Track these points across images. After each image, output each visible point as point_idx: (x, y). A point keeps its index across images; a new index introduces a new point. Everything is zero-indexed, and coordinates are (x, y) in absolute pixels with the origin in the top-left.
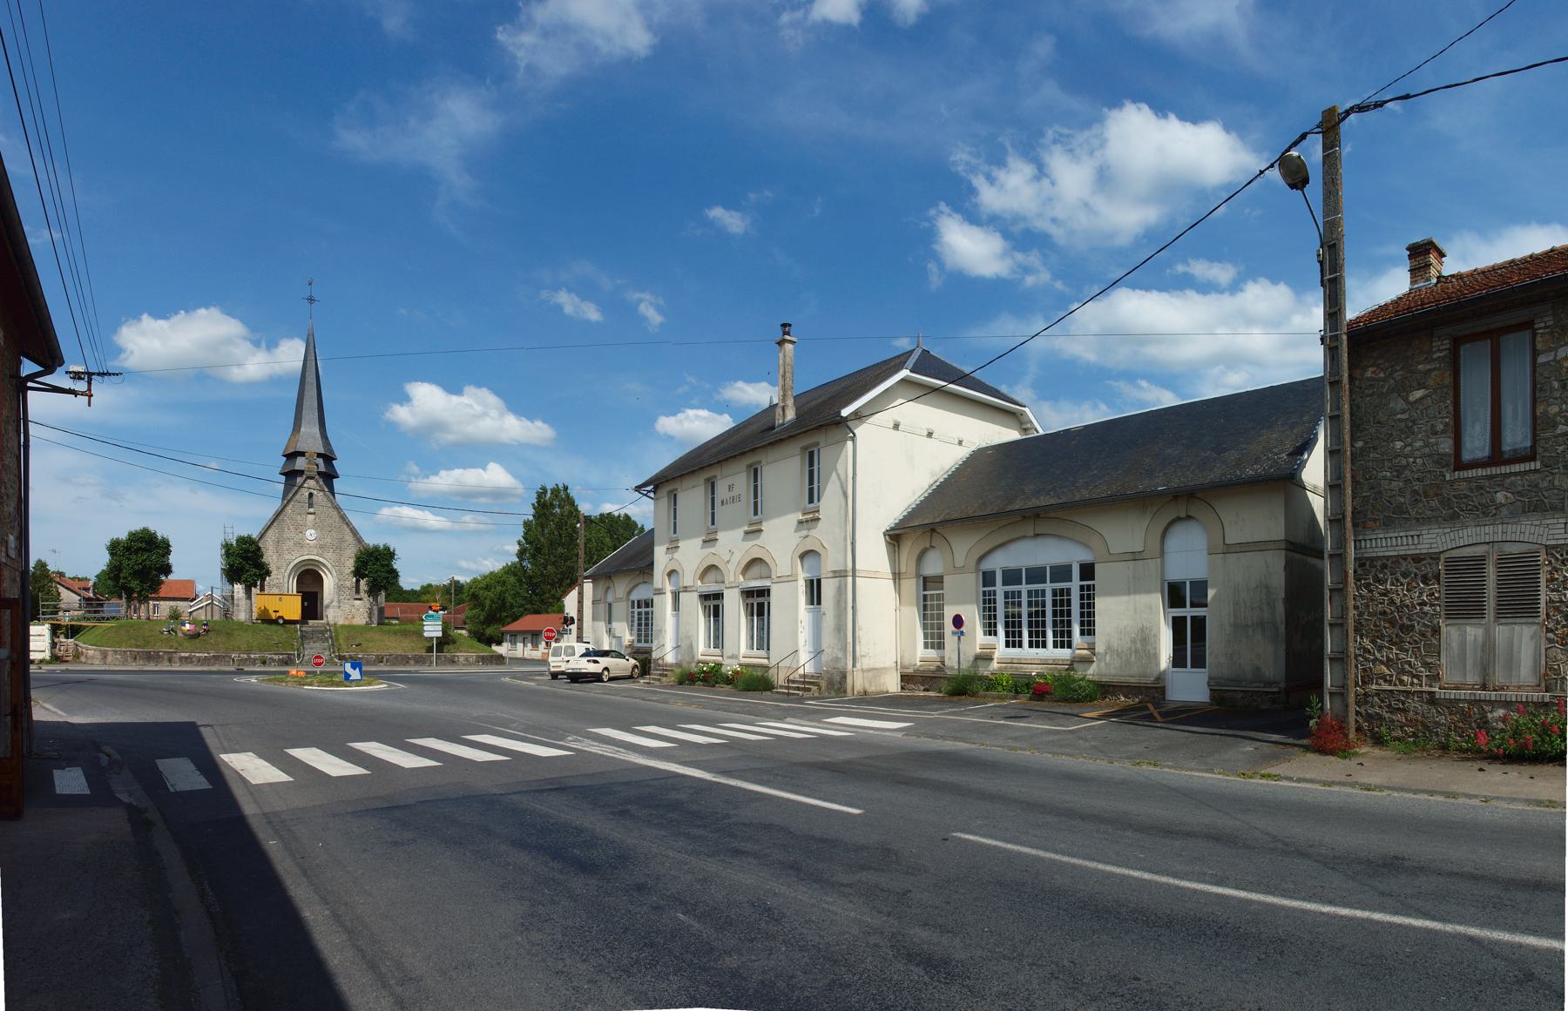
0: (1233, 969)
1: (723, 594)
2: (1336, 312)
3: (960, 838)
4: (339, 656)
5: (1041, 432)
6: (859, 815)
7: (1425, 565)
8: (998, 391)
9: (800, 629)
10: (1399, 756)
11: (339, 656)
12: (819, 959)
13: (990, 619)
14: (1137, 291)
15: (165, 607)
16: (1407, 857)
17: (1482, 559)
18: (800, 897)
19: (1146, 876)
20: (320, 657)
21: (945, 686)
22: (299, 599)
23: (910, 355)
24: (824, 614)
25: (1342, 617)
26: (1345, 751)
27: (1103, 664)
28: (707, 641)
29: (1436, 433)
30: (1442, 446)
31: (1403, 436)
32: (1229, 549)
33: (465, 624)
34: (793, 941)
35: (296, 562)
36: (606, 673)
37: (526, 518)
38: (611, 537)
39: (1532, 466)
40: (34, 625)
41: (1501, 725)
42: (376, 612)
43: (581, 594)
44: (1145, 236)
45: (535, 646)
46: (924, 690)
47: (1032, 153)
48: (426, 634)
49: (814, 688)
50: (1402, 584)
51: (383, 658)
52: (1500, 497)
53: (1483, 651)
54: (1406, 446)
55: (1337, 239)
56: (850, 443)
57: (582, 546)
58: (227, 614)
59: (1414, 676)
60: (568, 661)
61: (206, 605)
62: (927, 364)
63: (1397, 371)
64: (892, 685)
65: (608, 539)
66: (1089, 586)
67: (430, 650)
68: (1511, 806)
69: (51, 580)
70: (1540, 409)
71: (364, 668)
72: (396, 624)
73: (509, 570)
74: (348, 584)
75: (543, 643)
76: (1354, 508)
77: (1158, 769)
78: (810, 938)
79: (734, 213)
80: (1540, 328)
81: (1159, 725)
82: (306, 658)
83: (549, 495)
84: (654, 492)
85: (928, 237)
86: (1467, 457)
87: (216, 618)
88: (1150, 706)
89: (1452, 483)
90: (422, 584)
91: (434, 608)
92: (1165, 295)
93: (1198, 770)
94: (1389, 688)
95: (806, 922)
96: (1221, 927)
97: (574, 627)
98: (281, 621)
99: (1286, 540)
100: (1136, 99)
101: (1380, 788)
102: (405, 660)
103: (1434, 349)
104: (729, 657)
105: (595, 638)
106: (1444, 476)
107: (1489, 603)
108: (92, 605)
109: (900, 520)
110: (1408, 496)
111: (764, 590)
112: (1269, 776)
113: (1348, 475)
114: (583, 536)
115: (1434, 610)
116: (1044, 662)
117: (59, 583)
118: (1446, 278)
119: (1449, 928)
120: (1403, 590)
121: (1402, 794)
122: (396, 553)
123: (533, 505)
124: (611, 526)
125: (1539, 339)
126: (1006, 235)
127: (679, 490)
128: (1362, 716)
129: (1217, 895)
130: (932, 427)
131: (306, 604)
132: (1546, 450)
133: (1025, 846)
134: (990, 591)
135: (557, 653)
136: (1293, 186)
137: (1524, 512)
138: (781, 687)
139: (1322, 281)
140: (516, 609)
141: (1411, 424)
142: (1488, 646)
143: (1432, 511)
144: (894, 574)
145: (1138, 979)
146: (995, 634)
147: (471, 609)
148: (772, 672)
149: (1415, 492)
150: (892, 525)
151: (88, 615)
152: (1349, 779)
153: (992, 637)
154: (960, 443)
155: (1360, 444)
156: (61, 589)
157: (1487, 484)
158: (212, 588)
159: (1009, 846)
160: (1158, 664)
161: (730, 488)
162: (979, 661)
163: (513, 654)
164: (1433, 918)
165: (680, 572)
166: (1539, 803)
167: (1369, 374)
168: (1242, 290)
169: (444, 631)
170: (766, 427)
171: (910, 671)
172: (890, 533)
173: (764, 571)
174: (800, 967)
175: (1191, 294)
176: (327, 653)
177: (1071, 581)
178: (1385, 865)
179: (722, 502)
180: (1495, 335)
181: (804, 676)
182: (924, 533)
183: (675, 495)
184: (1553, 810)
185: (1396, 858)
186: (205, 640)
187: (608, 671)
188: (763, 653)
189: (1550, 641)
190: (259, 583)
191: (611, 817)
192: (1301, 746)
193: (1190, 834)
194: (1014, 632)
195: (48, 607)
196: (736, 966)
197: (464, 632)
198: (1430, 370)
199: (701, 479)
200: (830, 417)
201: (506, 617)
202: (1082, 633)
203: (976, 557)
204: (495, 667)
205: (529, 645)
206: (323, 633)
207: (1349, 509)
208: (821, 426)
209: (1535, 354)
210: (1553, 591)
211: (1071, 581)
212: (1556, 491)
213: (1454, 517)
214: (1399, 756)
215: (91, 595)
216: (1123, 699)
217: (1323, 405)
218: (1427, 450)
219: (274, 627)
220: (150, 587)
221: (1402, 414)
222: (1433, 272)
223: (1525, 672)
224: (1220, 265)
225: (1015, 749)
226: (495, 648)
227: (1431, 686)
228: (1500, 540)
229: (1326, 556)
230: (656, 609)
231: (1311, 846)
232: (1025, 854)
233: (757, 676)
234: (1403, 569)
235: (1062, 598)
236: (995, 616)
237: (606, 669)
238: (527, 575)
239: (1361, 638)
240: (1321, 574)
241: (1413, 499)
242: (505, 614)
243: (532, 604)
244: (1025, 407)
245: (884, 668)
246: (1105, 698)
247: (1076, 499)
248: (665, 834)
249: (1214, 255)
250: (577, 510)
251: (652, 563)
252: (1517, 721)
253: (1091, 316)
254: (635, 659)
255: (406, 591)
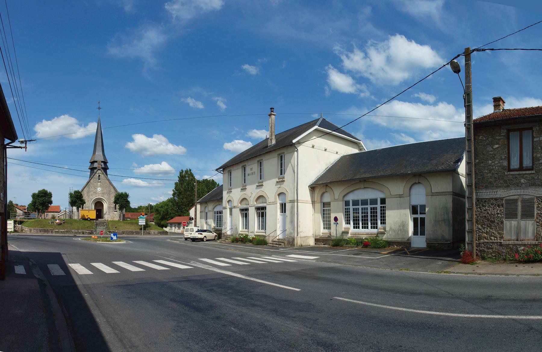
0: (435, 340)
1: (248, 209)
2: (470, 116)
3: (337, 299)
4: (109, 231)
5: (366, 150)
6: (299, 291)
7: (498, 201)
8: (351, 135)
9: (278, 222)
10: (490, 263)
11: (109, 231)
12: (284, 345)
13: (348, 218)
14: (401, 102)
15: (50, 215)
16: (493, 296)
17: (517, 200)
18: (277, 322)
19: (404, 309)
20: (102, 232)
21: (331, 243)
22: (95, 212)
23: (318, 120)
24: (287, 216)
25: (472, 218)
26: (472, 262)
27: (389, 234)
28: (243, 226)
29: (502, 159)
30: (504, 163)
31: (492, 159)
32: (433, 194)
33: (154, 220)
34: (274, 338)
35: (94, 199)
36: (205, 238)
37: (176, 181)
38: (207, 188)
39: (532, 172)
40: (9, 220)
41: (523, 252)
42: (122, 216)
43: (196, 209)
44: (404, 83)
45: (179, 228)
46: (324, 244)
47: (363, 48)
48: (140, 224)
49: (283, 244)
50: (491, 207)
51: (124, 232)
52: (522, 181)
53: (517, 229)
54: (492, 162)
55: (470, 92)
56: (296, 153)
57: (196, 192)
58: (71, 217)
59: (495, 237)
60: (191, 234)
61: (64, 214)
62: (325, 124)
63: (490, 138)
64: (312, 243)
65: (206, 189)
66: (383, 206)
67: (141, 229)
68: (526, 277)
69: (14, 207)
70: (535, 155)
71: (118, 236)
72: (129, 220)
73: (170, 201)
74: (112, 206)
75: (182, 227)
76: (475, 182)
77: (408, 271)
78: (281, 337)
79: (252, 67)
80: (535, 130)
81: (409, 256)
82: (98, 232)
83: (184, 173)
84: (223, 171)
85: (325, 77)
86: (512, 168)
87: (67, 218)
88: (406, 249)
89: (507, 175)
90: (138, 206)
91: (142, 214)
92: (411, 104)
93: (422, 271)
94: (487, 241)
95: (280, 331)
96: (430, 325)
97: (193, 221)
98: (89, 219)
99: (452, 192)
100: (401, 33)
101: (484, 274)
102: (132, 233)
103: (501, 132)
104: (251, 232)
105: (201, 225)
106: (505, 173)
107: (519, 213)
108: (27, 214)
109: (315, 181)
110: (493, 178)
111: (264, 207)
112: (447, 272)
113: (474, 171)
114: (197, 187)
115: (502, 216)
116: (367, 234)
117: (16, 208)
118: (505, 110)
119: (506, 317)
120: (491, 209)
121: (491, 275)
122: (129, 195)
123: (178, 176)
124: (207, 184)
125: (534, 133)
126: (354, 78)
127: (232, 170)
128: (478, 250)
129: (429, 314)
130: (326, 147)
131: (97, 213)
132: (536, 167)
133: (360, 301)
134: (347, 208)
135: (187, 231)
136: (455, 72)
137: (530, 186)
138: (270, 243)
139: (465, 105)
140: (172, 215)
141: (494, 156)
142: (519, 227)
143: (501, 184)
144: (312, 201)
145: (402, 346)
146: (350, 224)
147: (156, 215)
148: (267, 238)
149: (495, 178)
150: (312, 183)
151: (25, 218)
152: (474, 272)
153: (349, 225)
154: (337, 153)
155: (477, 161)
156: (17, 209)
157: (518, 176)
158: (66, 208)
159: (355, 301)
160: (408, 234)
161: (251, 169)
162: (343, 234)
163: (171, 231)
164: (501, 315)
165: (233, 202)
166: (534, 275)
167: (480, 138)
168: (437, 105)
169: (146, 223)
170: (264, 146)
171: (318, 237)
172: (311, 186)
173: (264, 201)
174: (277, 348)
175: (420, 104)
176: (105, 230)
177: (377, 205)
178: (486, 299)
179: (248, 175)
180: (521, 130)
181: (279, 239)
182: (323, 186)
183: (231, 172)
184: (539, 277)
185: (489, 296)
186: (63, 226)
187: (206, 237)
188: (263, 231)
189: (538, 225)
190: (81, 206)
191: (207, 291)
192: (458, 261)
193: (419, 294)
194: (356, 223)
195: (13, 215)
196: (253, 347)
197: (153, 223)
198: (500, 139)
199: (240, 167)
200: (289, 143)
201: (169, 217)
202: (381, 223)
203: (343, 195)
204: (164, 236)
205: (177, 228)
206: (103, 223)
207: (474, 182)
208: (285, 146)
209: (533, 138)
210: (538, 210)
211: (377, 205)
212: (539, 180)
213: (508, 186)
214: (490, 263)
215: (26, 211)
216: (396, 247)
217: (465, 147)
218: (499, 164)
219: (87, 221)
220: (45, 208)
221: (491, 152)
222: (501, 107)
223: (530, 235)
224: (430, 96)
225: (357, 266)
226: (164, 229)
227: (500, 240)
228: (522, 194)
229: (466, 197)
230: (224, 214)
231: (461, 295)
232: (360, 304)
233: (261, 239)
234: (491, 202)
235: (374, 211)
236: (350, 217)
237: (205, 237)
238: (176, 202)
239: (478, 225)
240: (464, 203)
241: (495, 180)
242: (168, 216)
243: (178, 213)
244: (360, 141)
245: (309, 237)
246: (390, 246)
247: (379, 175)
248: (227, 298)
249: (428, 92)
250: (194, 178)
251: (222, 198)
252: (527, 250)
253: (384, 109)
254: (216, 233)
255: (133, 209)
